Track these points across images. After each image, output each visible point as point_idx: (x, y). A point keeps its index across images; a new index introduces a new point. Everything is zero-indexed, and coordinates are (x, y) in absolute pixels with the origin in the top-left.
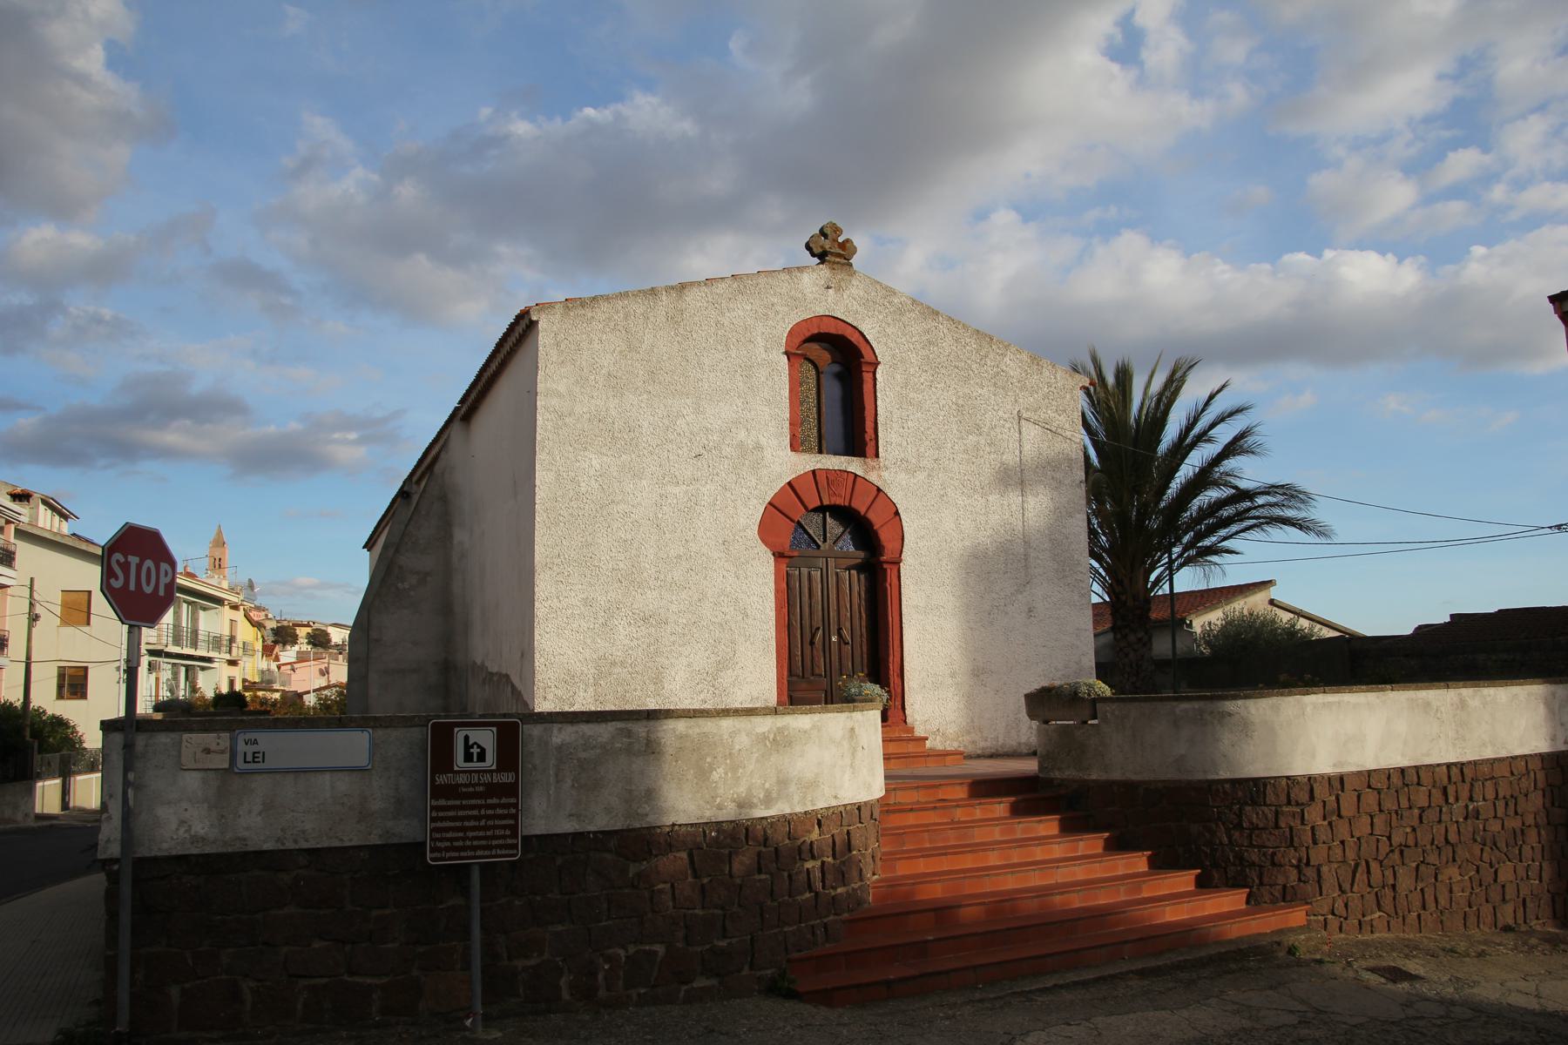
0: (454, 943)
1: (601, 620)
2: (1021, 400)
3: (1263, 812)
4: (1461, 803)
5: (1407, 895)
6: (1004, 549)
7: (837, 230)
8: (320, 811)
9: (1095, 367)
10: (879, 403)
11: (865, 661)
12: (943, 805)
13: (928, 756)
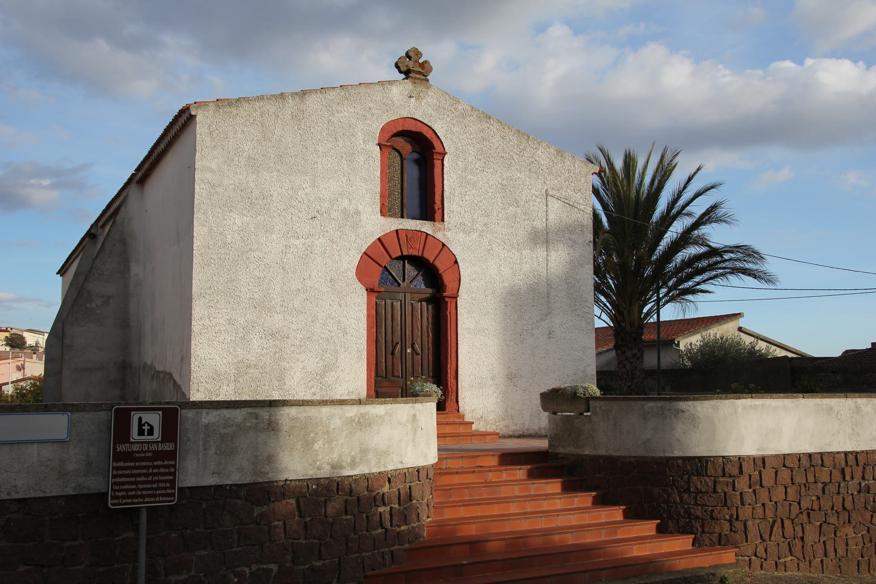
0: (126, 565)
1: (241, 335)
2: (549, 182)
3: (705, 481)
4: (856, 481)
5: (812, 545)
6: (533, 289)
7: (419, 54)
8: (28, 472)
9: (605, 157)
10: (445, 182)
11: (431, 367)
12: (480, 470)
13: (473, 435)
